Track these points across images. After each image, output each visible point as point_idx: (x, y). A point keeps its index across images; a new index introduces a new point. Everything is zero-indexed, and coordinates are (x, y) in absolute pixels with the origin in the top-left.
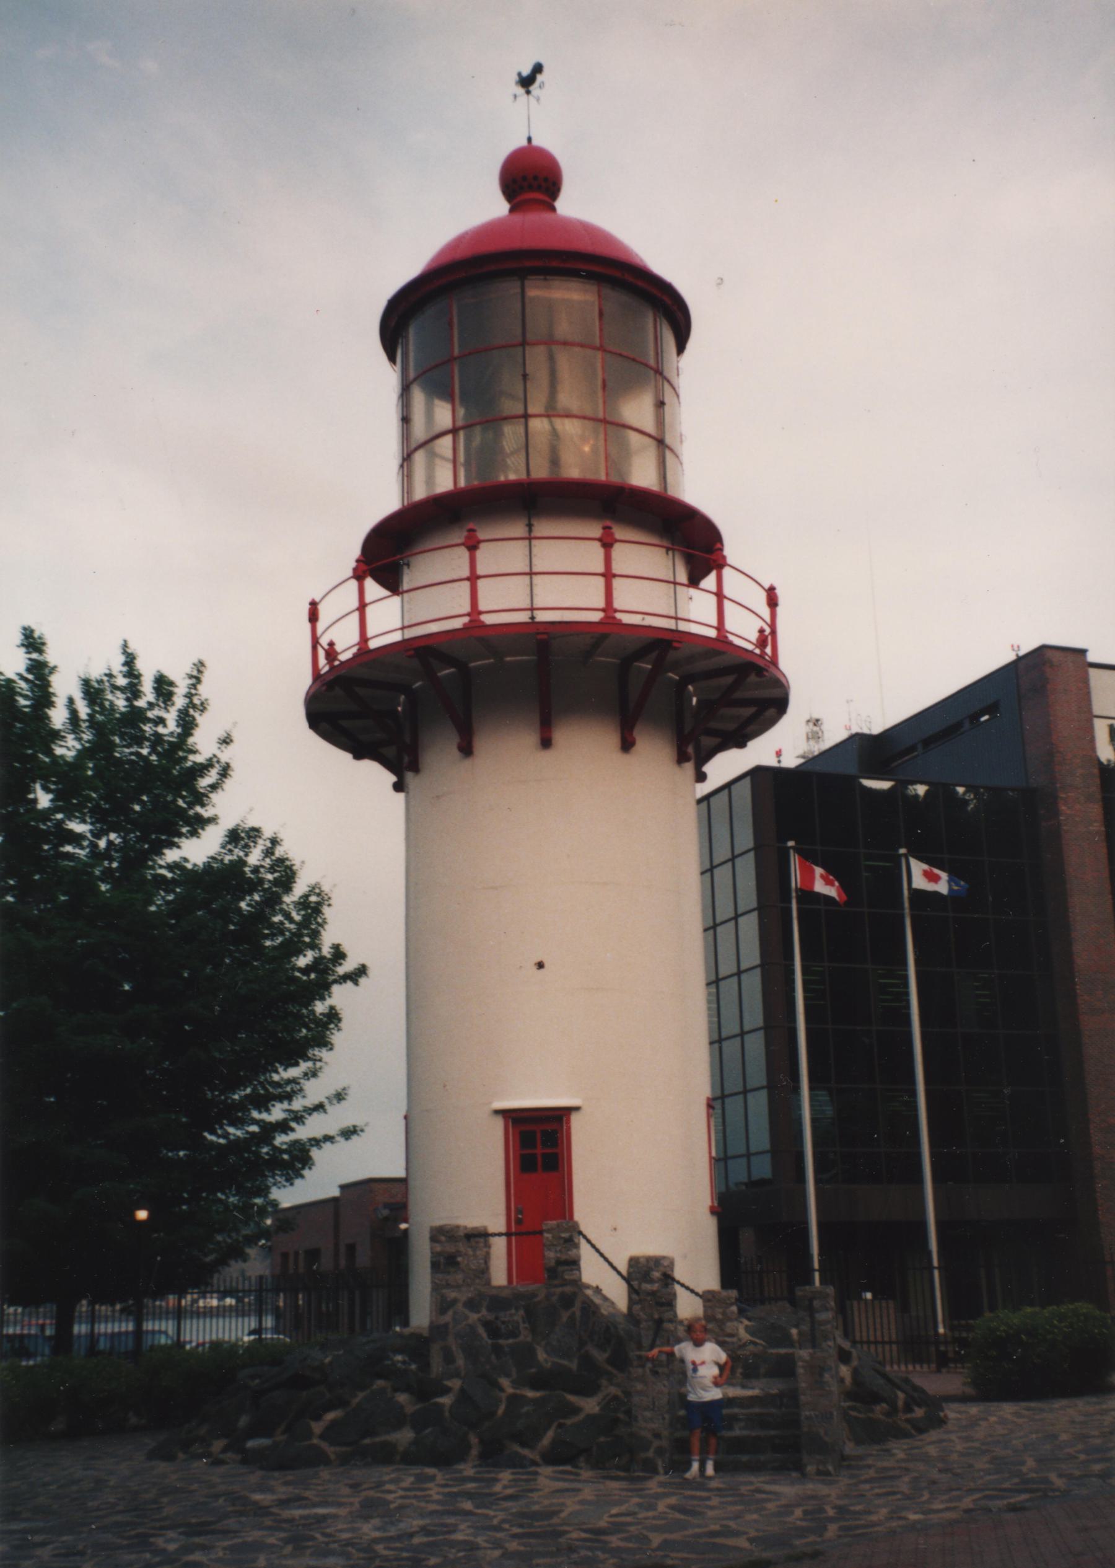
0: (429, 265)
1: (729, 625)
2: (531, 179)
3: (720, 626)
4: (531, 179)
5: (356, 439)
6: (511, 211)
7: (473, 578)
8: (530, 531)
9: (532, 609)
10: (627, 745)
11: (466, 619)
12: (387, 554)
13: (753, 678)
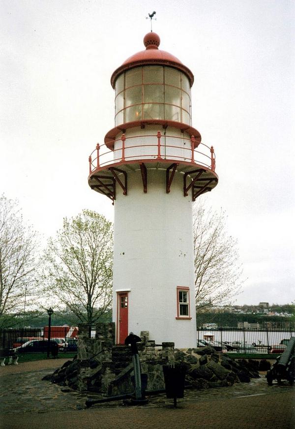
0: (127, 60)
1: (195, 158)
2: (152, 41)
3: (192, 159)
4: (152, 41)
5: (106, 108)
6: (147, 49)
7: (124, 148)
8: (165, 134)
9: (165, 156)
10: (145, 192)
11: (121, 160)
12: (111, 139)
13: (204, 173)
